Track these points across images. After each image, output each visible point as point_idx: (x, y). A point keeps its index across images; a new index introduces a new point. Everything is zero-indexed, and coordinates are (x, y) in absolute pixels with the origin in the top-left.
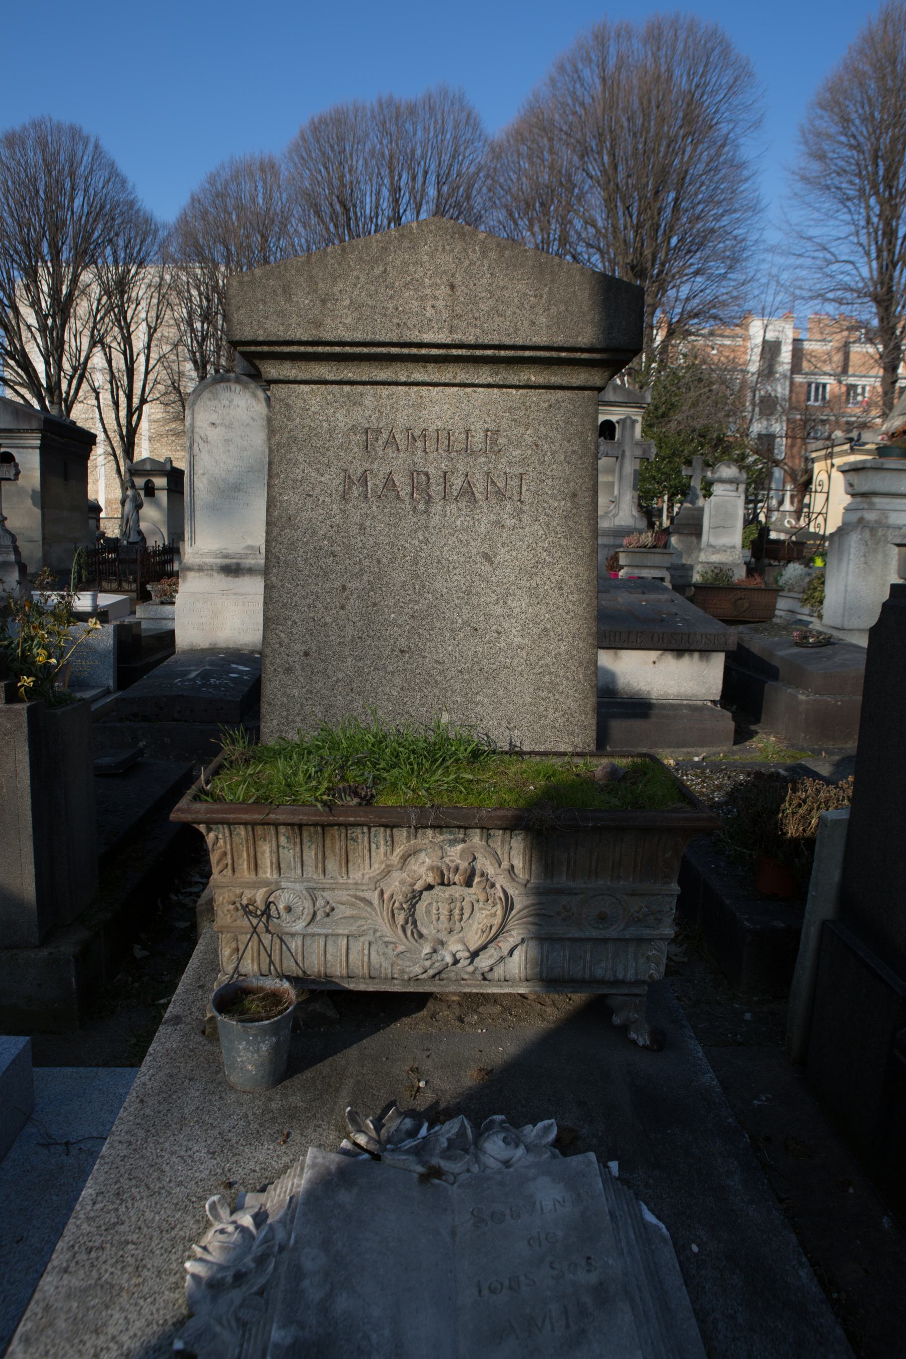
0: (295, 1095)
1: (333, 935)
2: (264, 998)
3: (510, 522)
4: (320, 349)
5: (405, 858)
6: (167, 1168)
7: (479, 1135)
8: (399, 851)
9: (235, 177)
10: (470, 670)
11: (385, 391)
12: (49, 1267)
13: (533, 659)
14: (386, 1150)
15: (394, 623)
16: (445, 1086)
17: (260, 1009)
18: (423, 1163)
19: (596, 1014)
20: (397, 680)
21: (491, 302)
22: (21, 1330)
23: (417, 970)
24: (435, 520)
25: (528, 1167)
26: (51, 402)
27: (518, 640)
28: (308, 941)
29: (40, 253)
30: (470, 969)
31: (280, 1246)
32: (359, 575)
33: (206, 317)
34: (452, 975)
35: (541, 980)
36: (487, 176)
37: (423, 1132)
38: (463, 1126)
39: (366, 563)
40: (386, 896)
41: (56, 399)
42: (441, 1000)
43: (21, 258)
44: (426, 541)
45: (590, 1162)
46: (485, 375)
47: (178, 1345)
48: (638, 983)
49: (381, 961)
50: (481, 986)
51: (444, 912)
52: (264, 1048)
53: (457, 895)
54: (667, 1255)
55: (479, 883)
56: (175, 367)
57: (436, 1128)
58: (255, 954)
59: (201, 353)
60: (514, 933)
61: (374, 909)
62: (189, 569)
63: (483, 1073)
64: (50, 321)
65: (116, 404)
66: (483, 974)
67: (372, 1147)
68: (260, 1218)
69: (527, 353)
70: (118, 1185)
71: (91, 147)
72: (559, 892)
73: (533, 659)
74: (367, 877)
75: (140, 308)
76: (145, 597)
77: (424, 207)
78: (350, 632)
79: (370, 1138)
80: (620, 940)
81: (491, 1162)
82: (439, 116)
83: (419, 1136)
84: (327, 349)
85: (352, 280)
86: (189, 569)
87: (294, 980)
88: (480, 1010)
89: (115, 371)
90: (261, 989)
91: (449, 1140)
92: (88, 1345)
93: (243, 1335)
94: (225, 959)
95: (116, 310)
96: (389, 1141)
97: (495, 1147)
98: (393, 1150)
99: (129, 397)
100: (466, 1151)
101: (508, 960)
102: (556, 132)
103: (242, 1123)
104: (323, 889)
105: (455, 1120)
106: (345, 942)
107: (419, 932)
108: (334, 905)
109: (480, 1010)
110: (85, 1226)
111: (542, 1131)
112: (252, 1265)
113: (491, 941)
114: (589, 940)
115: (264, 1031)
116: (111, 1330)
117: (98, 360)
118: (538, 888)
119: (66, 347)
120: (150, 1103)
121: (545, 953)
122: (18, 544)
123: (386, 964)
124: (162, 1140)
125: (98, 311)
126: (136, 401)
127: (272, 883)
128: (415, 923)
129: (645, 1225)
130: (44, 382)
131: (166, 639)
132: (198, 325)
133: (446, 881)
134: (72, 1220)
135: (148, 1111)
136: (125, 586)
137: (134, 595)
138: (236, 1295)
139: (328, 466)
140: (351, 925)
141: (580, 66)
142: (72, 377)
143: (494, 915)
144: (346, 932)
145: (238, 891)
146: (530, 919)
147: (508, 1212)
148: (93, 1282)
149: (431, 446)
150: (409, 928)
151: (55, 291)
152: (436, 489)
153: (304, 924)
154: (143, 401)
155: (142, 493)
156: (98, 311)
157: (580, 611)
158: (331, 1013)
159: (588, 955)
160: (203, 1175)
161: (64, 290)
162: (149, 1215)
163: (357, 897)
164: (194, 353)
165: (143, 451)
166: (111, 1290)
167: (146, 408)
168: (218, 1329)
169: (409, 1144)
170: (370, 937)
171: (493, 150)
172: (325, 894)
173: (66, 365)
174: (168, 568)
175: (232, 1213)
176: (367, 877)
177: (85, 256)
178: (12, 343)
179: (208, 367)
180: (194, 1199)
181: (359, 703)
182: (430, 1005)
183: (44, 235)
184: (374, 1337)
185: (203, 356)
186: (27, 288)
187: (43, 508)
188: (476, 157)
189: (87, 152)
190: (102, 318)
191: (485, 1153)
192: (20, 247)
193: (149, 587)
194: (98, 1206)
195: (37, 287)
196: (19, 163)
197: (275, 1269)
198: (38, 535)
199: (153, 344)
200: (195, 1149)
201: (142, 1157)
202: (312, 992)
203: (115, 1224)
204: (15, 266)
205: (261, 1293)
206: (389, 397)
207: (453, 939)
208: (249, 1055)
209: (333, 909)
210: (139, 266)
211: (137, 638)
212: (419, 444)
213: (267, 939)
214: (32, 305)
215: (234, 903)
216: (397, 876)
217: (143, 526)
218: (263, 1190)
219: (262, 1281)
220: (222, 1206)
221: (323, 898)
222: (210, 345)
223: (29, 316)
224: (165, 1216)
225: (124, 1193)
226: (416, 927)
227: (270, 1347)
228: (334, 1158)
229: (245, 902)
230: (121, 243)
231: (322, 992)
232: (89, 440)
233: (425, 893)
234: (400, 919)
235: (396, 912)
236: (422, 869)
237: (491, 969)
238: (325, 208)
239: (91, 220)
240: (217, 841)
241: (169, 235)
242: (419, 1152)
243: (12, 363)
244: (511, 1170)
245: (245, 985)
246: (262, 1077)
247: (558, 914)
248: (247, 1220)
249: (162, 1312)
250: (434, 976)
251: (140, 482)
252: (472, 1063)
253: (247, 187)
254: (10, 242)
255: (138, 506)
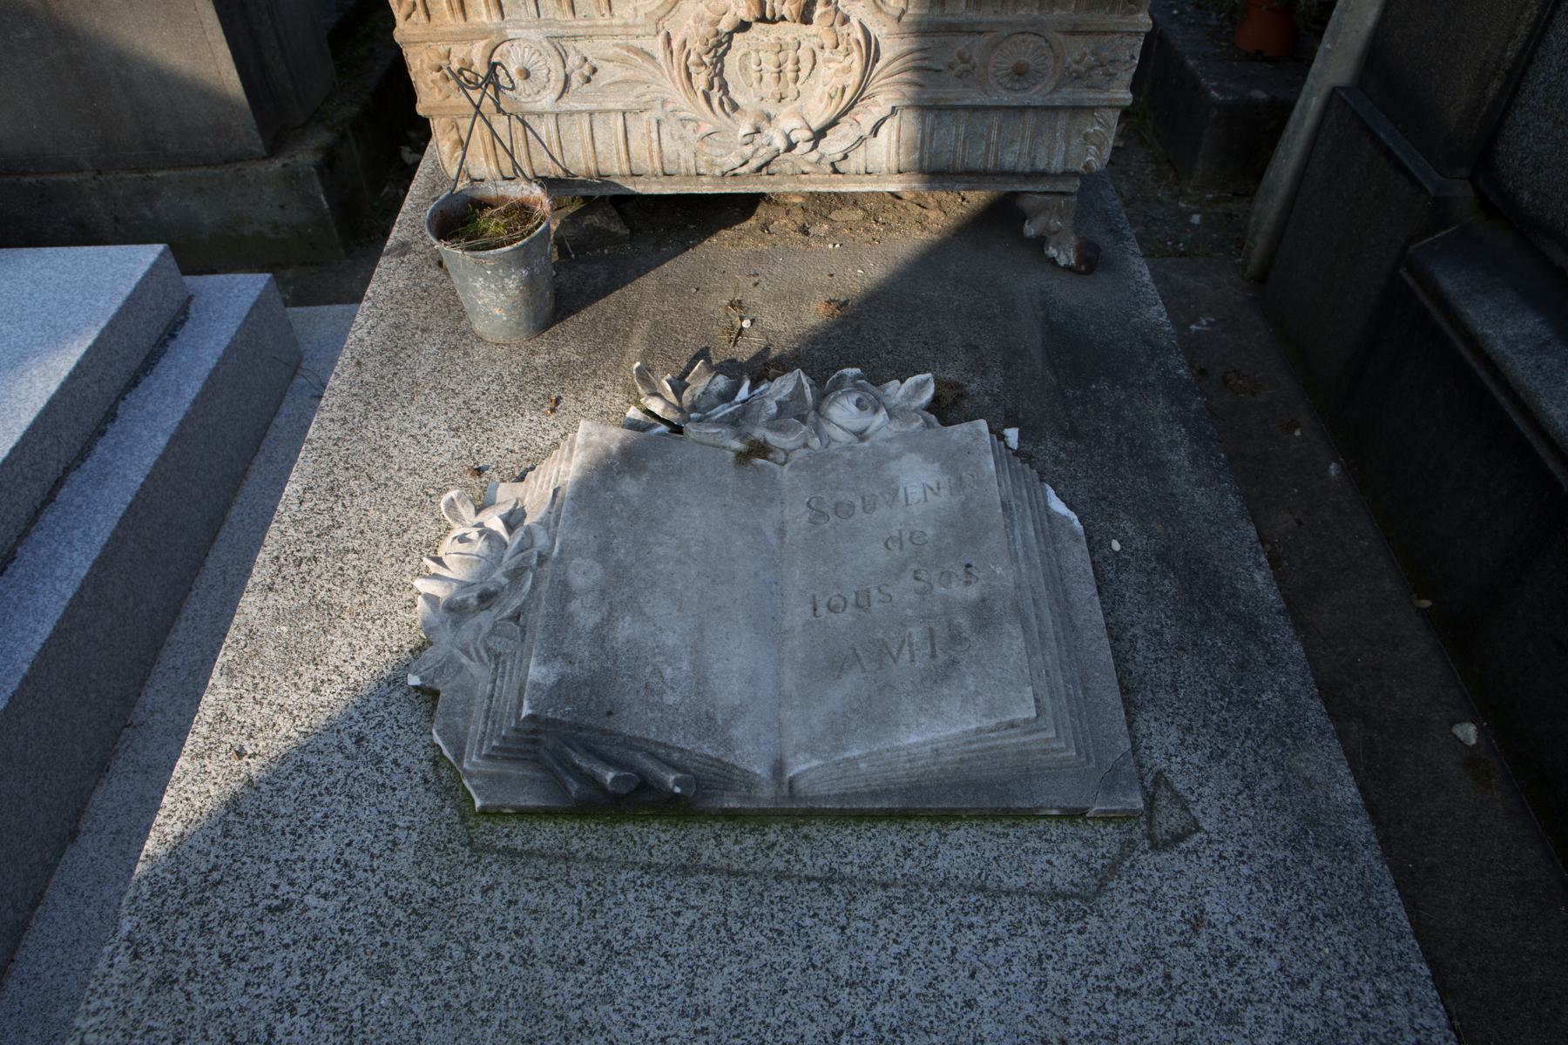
0: (568, 342)
1: (600, 112)
2: (506, 214)
6: (395, 452)
7: (822, 397)
12: (250, 584)
14: (689, 420)
16: (778, 326)
17: (501, 229)
18: (742, 437)
19: (1001, 219)
22: (221, 660)
23: (733, 161)
25: (890, 440)
28: (565, 123)
30: (814, 156)
31: (540, 555)
34: (787, 167)
35: (921, 171)
37: (743, 393)
38: (799, 383)
40: (675, 44)
42: (777, 203)
45: (979, 433)
47: (414, 680)
48: (1066, 175)
50: (831, 182)
51: (770, 68)
52: (512, 284)
53: (788, 39)
54: (1078, 557)
55: (822, 15)
57: (762, 388)
58: (489, 148)
60: (880, 99)
61: (659, 67)
63: (833, 306)
66: (833, 164)
67: (670, 415)
68: (513, 520)
70: (332, 477)
72: (954, 29)
74: (641, 12)
79: (668, 403)
80: (1046, 108)
81: (839, 434)
83: (737, 399)
87: (548, 183)
88: (833, 216)
90: (504, 199)
91: (779, 403)
92: (305, 677)
93: (496, 669)
94: (445, 159)
96: (694, 408)
97: (844, 413)
98: (700, 420)
100: (803, 419)
101: (871, 141)
103: (494, 386)
104: (575, 37)
105: (789, 375)
106: (620, 122)
107: (731, 100)
108: (595, 63)
109: (833, 216)
110: (291, 531)
111: (914, 390)
112: (505, 581)
113: (844, 113)
115: (506, 262)
116: (333, 660)
118: (919, 24)
120: (370, 366)
121: (928, 130)
123: (686, 154)
124: (387, 415)
127: (491, 32)
128: (724, 86)
129: (1051, 516)
133: (768, 15)
134: (274, 525)
135: (367, 377)
138: (485, 619)
140: (626, 94)
143: (849, 70)
144: (619, 106)
145: (442, 49)
146: (906, 76)
147: (858, 503)
148: (306, 602)
150: (716, 95)
153: (554, 96)
158: (618, 228)
159: (995, 132)
160: (444, 460)
162: (373, 515)
163: (629, 49)
166: (330, 612)
168: (464, 660)
169: (723, 410)
172: (579, 45)
175: (478, 511)
176: (641, 12)
180: (432, 492)
182: (761, 211)
184: (668, 672)
191: (830, 421)
194: (306, 506)
197: (534, 586)
200: (431, 425)
201: (362, 438)
202: (587, 199)
203: (329, 528)
205: (516, 617)
207: (785, 111)
208: (492, 295)
209: (594, 70)
213: (500, 124)
215: (440, 69)
218: (521, 479)
219: (516, 602)
220: (464, 503)
221: (578, 52)
224: (393, 515)
225: (339, 486)
226: (726, 92)
227: (527, 687)
228: (615, 436)
229: (455, 66)
231: (602, 198)
233: (737, 36)
234: (701, 81)
235: (692, 69)
237: (845, 157)
242: (734, 422)
244: (866, 444)
245: (478, 194)
246: (518, 324)
247: (951, 67)
248: (494, 522)
249: (395, 637)
250: (759, 169)
252: (818, 293)
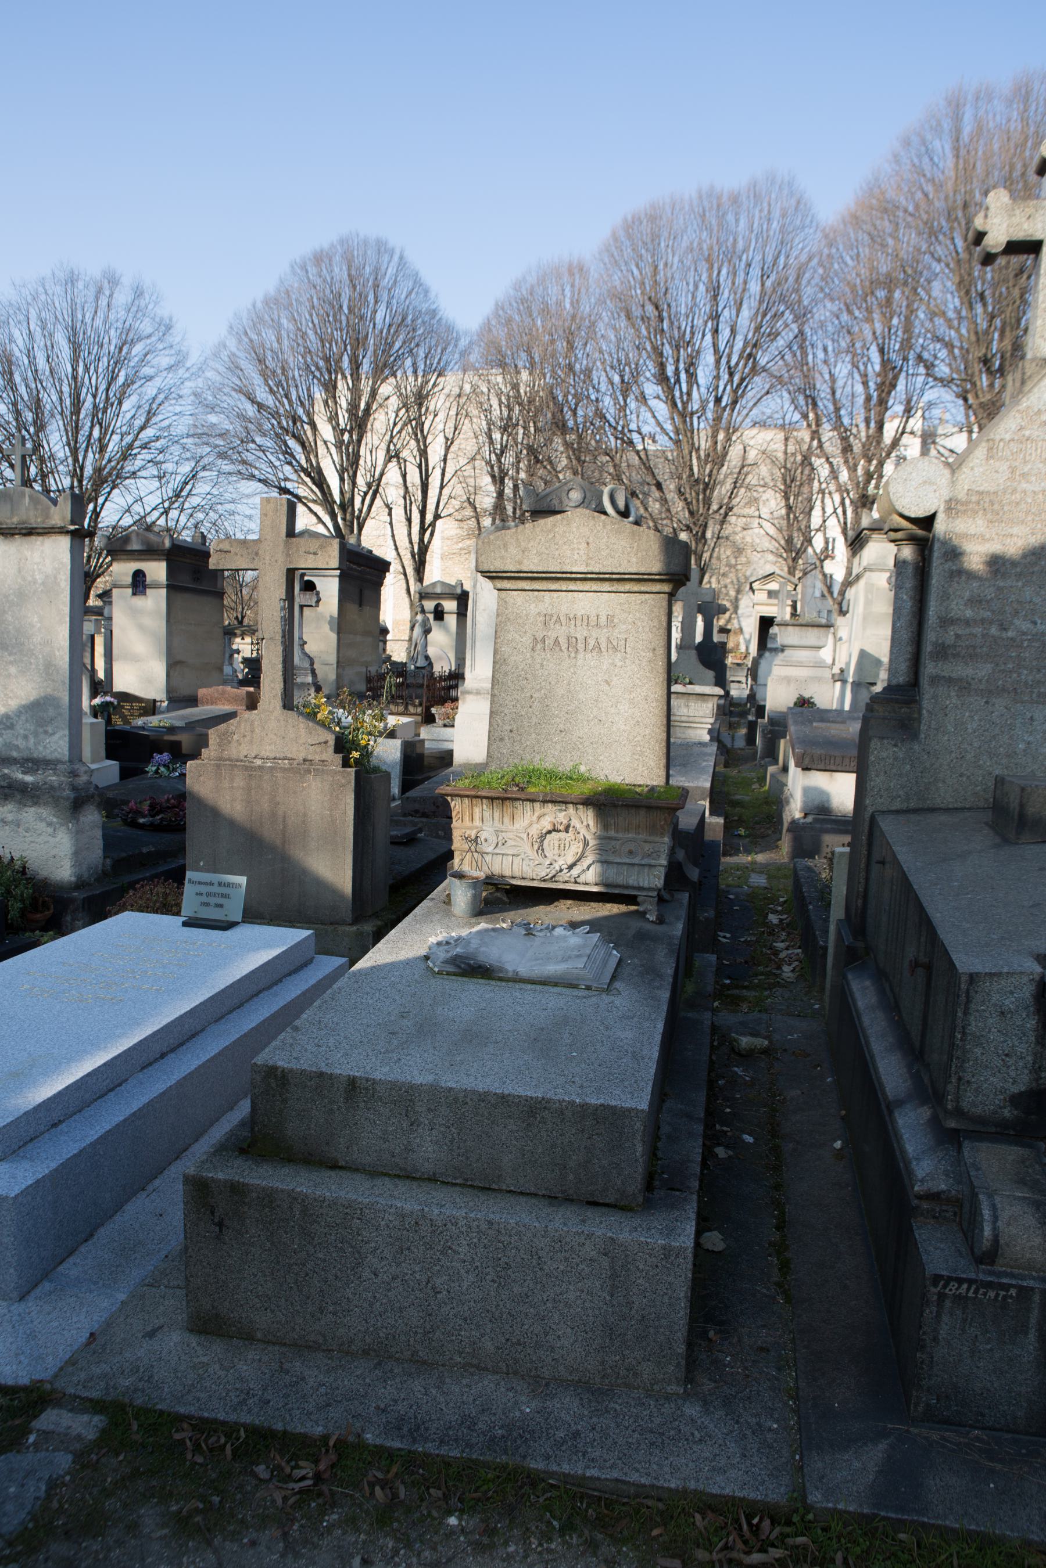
3: (619, 664)
4: (521, 575)
5: (539, 818)
8: (537, 814)
9: (542, 280)
10: (596, 743)
11: (555, 594)
13: (631, 737)
15: (557, 716)
20: (558, 747)
21: (608, 551)
24: (580, 662)
26: (344, 519)
27: (623, 727)
29: (340, 368)
32: (539, 690)
33: (507, 427)
36: (821, 264)
39: (543, 684)
41: (348, 517)
43: (321, 373)
44: (575, 673)
46: (606, 586)
49: (528, 872)
51: (557, 845)
52: (469, 895)
56: (471, 481)
59: (500, 467)
62: (468, 692)
64: (346, 437)
65: (409, 520)
69: (627, 576)
71: (396, 258)
72: (610, 838)
73: (631, 737)
75: (437, 419)
76: (429, 719)
77: (745, 306)
78: (534, 720)
82: (765, 205)
84: (525, 575)
85: (537, 540)
86: (468, 692)
89: (409, 484)
95: (414, 423)
99: (423, 513)
102: (901, 214)
114: (625, 864)
117: (393, 474)
119: (362, 462)
122: (315, 666)
123: (530, 871)
125: (395, 424)
126: (429, 517)
130: (337, 498)
131: (446, 758)
132: (497, 436)
136: (411, 709)
137: (419, 718)
139: (525, 633)
141: (929, 137)
142: (366, 494)
149: (579, 623)
151: (353, 407)
152: (581, 646)
154: (437, 517)
155: (431, 617)
156: (395, 424)
157: (657, 712)
158: (505, 899)
161: (363, 406)
164: (492, 467)
165: (434, 573)
167: (439, 523)
170: (523, 856)
171: (826, 236)
173: (361, 481)
174: (453, 693)
177: (383, 369)
178: (308, 460)
179: (506, 481)
181: (538, 758)
183: (346, 350)
185: (501, 470)
186: (326, 403)
187: (339, 633)
188: (806, 245)
189: (391, 264)
190: (400, 432)
192: (321, 363)
193: (433, 710)
195: (336, 403)
196: (325, 281)
198: (333, 659)
199: (449, 456)
204: (315, 381)
206: (558, 597)
210: (439, 375)
211: (421, 756)
212: (573, 622)
214: (330, 420)
216: (535, 826)
217: (431, 651)
222: (508, 459)
223: (326, 431)
230: (422, 354)
232: (381, 567)
234: (536, 847)
236: (546, 824)
238: (637, 312)
239: (392, 331)
240: (456, 805)
241: (471, 343)
243: (307, 480)
251: (429, 605)
253: (554, 290)
254: (312, 359)
255: (427, 631)
